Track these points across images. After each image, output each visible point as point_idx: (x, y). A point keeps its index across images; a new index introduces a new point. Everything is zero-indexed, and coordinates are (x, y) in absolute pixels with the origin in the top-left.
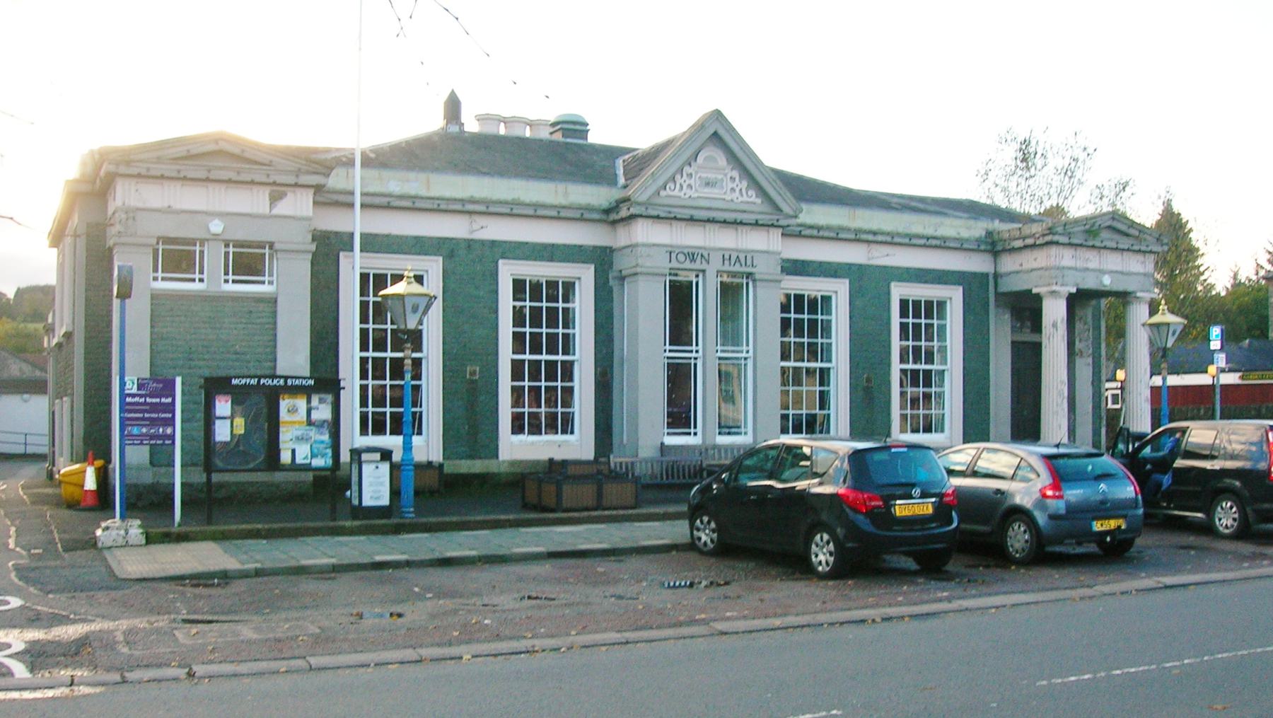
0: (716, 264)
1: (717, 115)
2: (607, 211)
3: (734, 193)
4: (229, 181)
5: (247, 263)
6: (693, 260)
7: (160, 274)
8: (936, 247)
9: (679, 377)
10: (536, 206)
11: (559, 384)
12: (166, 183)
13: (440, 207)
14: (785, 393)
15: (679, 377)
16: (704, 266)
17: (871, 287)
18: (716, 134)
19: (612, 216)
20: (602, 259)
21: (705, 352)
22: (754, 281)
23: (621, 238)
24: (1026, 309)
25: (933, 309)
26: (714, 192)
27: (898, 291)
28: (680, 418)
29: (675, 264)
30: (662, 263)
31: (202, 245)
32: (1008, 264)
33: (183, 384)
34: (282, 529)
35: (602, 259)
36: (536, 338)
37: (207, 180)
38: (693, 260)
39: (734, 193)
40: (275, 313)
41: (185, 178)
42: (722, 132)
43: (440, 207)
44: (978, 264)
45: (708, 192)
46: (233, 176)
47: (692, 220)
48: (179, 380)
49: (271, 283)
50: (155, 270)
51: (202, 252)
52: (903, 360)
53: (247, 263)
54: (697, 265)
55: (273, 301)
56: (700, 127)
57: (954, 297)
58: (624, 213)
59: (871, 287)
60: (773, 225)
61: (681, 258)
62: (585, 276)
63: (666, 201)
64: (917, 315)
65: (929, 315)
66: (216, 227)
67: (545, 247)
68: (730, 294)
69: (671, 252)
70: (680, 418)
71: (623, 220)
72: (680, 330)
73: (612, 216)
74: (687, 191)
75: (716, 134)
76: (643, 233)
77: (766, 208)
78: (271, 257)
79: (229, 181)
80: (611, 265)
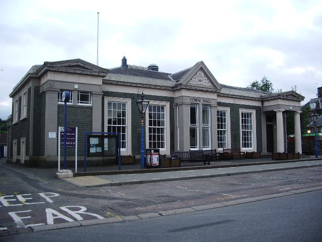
0: (202, 102)
1: (202, 62)
2: (173, 88)
3: (206, 83)
4: (80, 74)
5: (84, 97)
6: (196, 101)
7: (79, 101)
8: (163, 89)
9: (193, 132)
10: (252, 98)
11: (156, 134)
12: (62, 74)
13: (131, 85)
14: (218, 137)
15: (193, 132)
16: (199, 103)
17: (234, 108)
18: (201, 68)
19: (174, 89)
20: (171, 100)
21: (199, 126)
22: (211, 107)
23: (177, 94)
24: (271, 117)
25: (249, 115)
26: (200, 83)
27: (241, 111)
28: (193, 144)
29: (192, 102)
30: (188, 101)
31: (72, 92)
32: (266, 104)
33: (78, 130)
34: (135, 171)
35: (171, 100)
36: (155, 121)
37: (74, 73)
38: (196, 101)
39: (206, 83)
40: (92, 112)
41: (68, 73)
42: (203, 67)
43: (131, 85)
44: (258, 104)
45: (200, 83)
46: (81, 72)
47: (202, 91)
48: (77, 128)
49: (90, 103)
50: (78, 100)
51: (72, 94)
52: (150, 124)
53: (84, 97)
54: (197, 102)
55: (91, 108)
56: (198, 64)
57: (254, 112)
58: (179, 88)
59: (234, 108)
60: (215, 92)
61: (193, 100)
62: (167, 105)
63: (189, 85)
64: (155, 111)
65: (159, 111)
66: (76, 87)
67: (125, 94)
68: (205, 112)
69: (191, 98)
70: (193, 144)
71: (178, 90)
72: (193, 121)
73: (174, 89)
74: (194, 82)
75: (201, 68)
76: (184, 93)
77: (213, 88)
78: (90, 96)
79: (80, 74)
80: (173, 102)
